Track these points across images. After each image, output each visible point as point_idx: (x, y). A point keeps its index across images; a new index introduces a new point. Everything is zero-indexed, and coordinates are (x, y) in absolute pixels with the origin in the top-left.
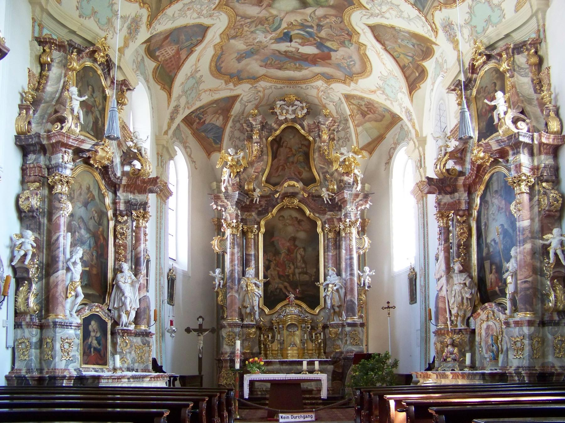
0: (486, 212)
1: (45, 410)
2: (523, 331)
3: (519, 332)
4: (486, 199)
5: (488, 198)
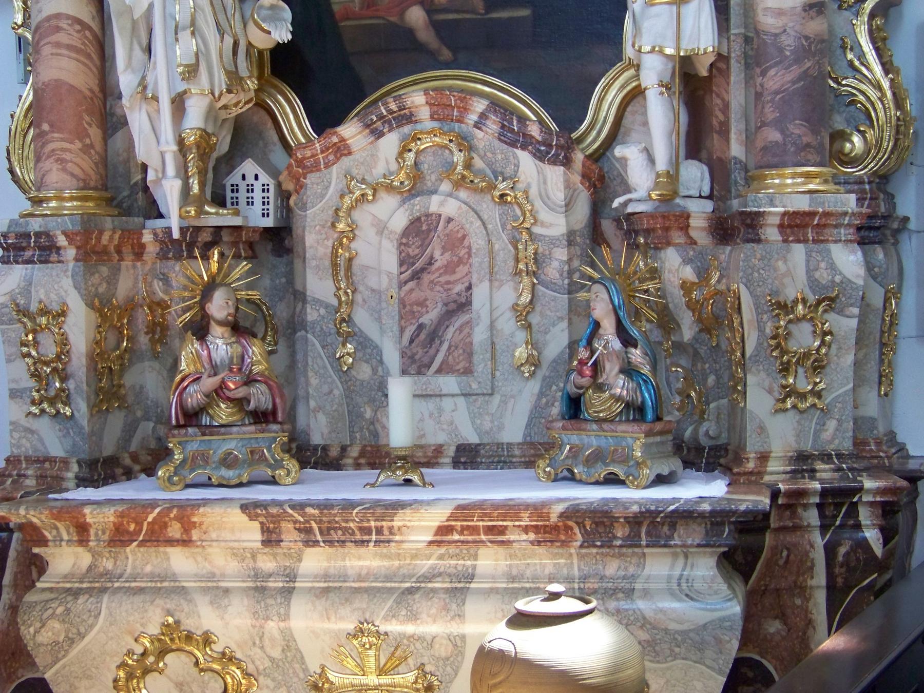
2: (832, 267)
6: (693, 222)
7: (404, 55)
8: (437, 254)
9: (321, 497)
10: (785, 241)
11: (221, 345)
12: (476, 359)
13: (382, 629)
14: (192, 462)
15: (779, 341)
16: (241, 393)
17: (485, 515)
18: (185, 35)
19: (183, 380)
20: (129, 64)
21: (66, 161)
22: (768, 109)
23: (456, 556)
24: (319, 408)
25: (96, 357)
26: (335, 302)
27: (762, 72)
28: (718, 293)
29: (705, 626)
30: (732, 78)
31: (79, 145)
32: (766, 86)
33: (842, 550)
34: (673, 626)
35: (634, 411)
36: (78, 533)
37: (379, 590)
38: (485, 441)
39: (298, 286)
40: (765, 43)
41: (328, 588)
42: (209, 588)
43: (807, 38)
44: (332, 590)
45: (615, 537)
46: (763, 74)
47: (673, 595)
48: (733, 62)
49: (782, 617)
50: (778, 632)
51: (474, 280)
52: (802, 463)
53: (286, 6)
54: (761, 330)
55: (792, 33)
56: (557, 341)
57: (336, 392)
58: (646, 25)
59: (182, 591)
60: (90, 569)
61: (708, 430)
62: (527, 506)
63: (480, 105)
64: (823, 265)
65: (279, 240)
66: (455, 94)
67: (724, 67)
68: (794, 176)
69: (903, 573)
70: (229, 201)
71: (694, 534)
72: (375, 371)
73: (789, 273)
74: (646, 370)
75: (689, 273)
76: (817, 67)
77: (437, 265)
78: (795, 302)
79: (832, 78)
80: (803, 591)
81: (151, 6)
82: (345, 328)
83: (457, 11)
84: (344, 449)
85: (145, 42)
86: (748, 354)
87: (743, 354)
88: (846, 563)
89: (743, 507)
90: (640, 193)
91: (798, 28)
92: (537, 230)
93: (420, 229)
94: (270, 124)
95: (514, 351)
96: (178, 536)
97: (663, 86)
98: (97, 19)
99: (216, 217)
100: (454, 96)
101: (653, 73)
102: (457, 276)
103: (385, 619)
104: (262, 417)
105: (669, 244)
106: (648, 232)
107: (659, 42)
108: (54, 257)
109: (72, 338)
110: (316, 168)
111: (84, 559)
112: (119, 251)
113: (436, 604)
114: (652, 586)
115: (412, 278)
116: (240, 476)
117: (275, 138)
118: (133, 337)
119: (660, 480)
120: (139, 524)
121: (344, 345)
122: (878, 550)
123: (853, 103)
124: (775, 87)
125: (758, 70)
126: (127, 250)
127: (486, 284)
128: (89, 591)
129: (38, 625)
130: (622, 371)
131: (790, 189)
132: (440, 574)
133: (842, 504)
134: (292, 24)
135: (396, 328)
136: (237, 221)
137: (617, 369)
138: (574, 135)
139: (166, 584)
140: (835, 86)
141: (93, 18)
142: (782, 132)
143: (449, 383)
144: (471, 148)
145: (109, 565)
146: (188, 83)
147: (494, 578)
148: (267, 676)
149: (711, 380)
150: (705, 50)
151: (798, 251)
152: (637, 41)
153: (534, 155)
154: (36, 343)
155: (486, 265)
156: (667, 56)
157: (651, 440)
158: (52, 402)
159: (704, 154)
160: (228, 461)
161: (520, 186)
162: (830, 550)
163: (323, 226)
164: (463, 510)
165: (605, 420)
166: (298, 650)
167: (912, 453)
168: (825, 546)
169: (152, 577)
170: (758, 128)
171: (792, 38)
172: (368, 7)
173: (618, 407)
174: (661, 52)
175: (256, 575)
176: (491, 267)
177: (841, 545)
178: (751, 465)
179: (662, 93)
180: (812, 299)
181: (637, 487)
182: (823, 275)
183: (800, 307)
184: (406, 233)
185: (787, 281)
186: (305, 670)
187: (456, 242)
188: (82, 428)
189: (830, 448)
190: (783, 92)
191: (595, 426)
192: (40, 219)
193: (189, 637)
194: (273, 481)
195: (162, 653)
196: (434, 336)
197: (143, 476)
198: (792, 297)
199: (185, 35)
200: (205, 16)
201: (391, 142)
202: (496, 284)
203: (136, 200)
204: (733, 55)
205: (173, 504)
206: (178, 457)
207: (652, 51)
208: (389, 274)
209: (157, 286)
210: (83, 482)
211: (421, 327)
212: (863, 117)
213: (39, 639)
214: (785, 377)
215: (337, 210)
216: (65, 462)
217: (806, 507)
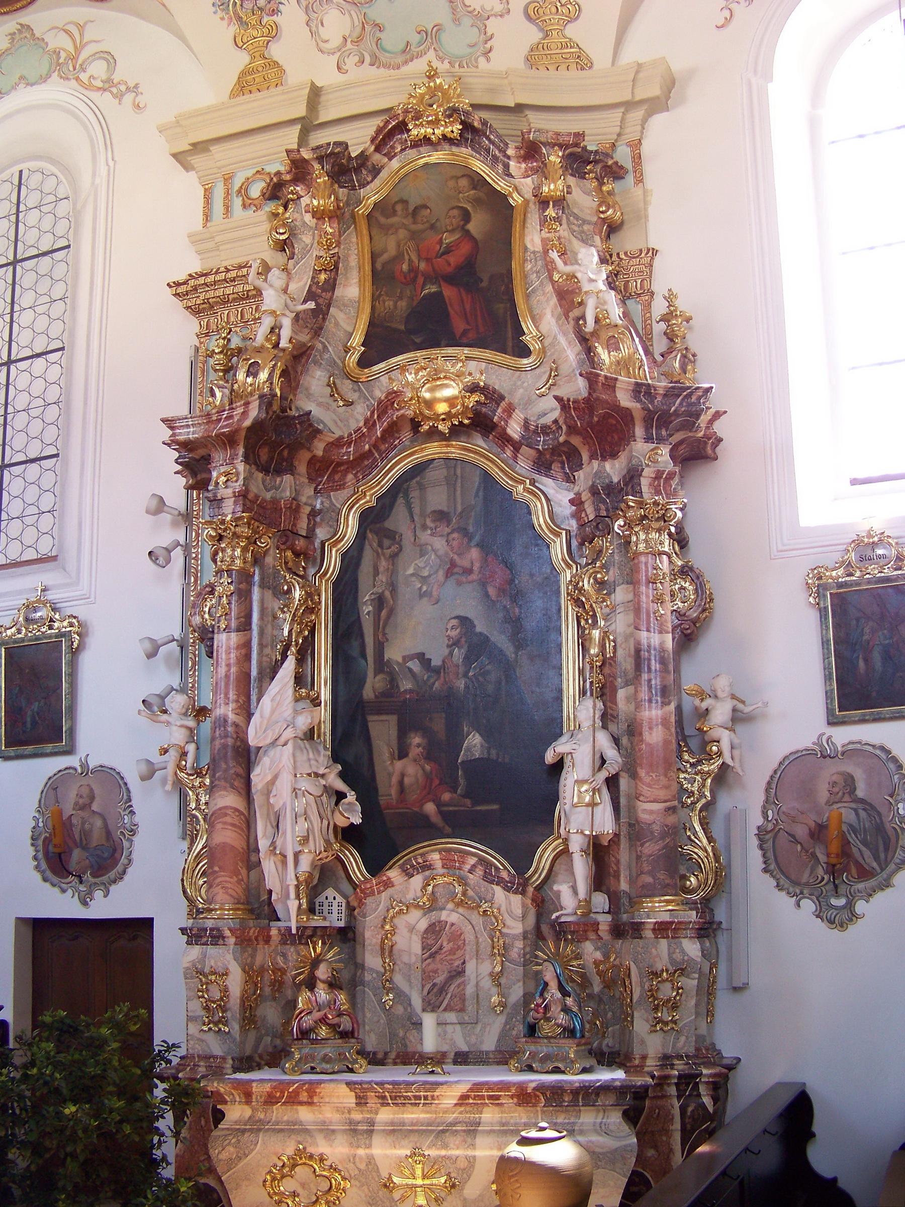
0: (383, 564)
1: (407, 852)
2: (683, 952)
3: (670, 955)
4: (389, 524)
5: (399, 520)
6: (601, 927)
7: (422, 830)
8: (445, 944)
9: (390, 1079)
10: (656, 938)
11: (322, 994)
12: (467, 1003)
13: (426, 1153)
14: (303, 1060)
15: (652, 993)
16: (336, 1021)
17: (490, 1088)
18: (301, 820)
19: (300, 1013)
20: (264, 835)
21: (227, 888)
22: (645, 865)
23: (470, 1112)
24: (371, 1030)
25: (243, 1000)
26: (382, 970)
28: (614, 966)
29: (616, 1150)
31: (235, 879)
33: (690, 1109)
34: (597, 1150)
35: (570, 1032)
36: (246, 1097)
37: (424, 1131)
38: (472, 1050)
39: (359, 961)
41: (393, 1130)
42: (323, 1129)
43: (667, 826)
44: (396, 1131)
45: (564, 1101)
46: (642, 845)
47: (596, 1131)
49: (655, 1147)
50: (653, 1155)
51: (467, 958)
52: (666, 1060)
54: (642, 987)
56: (517, 993)
57: (382, 1021)
58: (573, 818)
59: (307, 1131)
60: (250, 1117)
61: (608, 1043)
62: (514, 1084)
63: (472, 861)
64: (677, 951)
65: (347, 935)
68: (660, 902)
69: (721, 1125)
70: (317, 911)
71: (611, 1099)
72: (405, 1009)
73: (658, 956)
74: (575, 1009)
75: (598, 955)
77: (445, 950)
78: (662, 971)
80: (667, 1132)
82: (387, 984)
83: (455, 806)
84: (386, 1054)
85: (275, 824)
86: (634, 1001)
87: (631, 1000)
88: (692, 1116)
89: (639, 1083)
90: (569, 910)
91: (662, 820)
92: (505, 930)
93: (434, 930)
94: (340, 867)
95: (490, 999)
96: (305, 1100)
99: (317, 921)
101: (576, 844)
102: (455, 957)
103: (429, 1147)
104: (345, 1035)
105: (587, 939)
106: (572, 933)
107: (581, 827)
108: (221, 942)
109: (231, 988)
110: (372, 893)
111: (247, 1112)
112: (256, 939)
113: (458, 1140)
114: (585, 1128)
115: (430, 957)
116: (333, 1068)
117: (343, 875)
118: (269, 986)
119: (585, 1070)
120: (282, 1092)
121: (388, 995)
122: (711, 1110)
123: (691, 859)
124: (650, 852)
125: (639, 843)
126: (260, 938)
127: (474, 960)
128: (251, 1130)
129: (220, 1149)
130: (562, 1010)
131: (658, 909)
132: (460, 1122)
133: (689, 1084)
135: (420, 986)
136: (327, 924)
137: (559, 1009)
138: (527, 876)
139: (296, 1127)
142: (654, 878)
143: (451, 1017)
144: (466, 884)
145: (262, 1116)
147: (492, 1124)
148: (356, 1179)
149: (610, 1014)
151: (664, 943)
153: (504, 889)
154: (207, 990)
155: (474, 950)
157: (580, 1048)
158: (216, 1024)
159: (604, 888)
160: (326, 1059)
161: (495, 905)
162: (683, 1109)
163: (376, 927)
164: (477, 1086)
165: (551, 1037)
166: (376, 1164)
167: (724, 1055)
168: (680, 1107)
169: (288, 1123)
170: (638, 876)
173: (559, 1030)
174: (582, 832)
175: (350, 1123)
176: (477, 951)
177: (688, 1106)
178: (637, 1062)
180: (671, 970)
181: (572, 1074)
182: (678, 956)
183: (665, 974)
184: (426, 931)
185: (657, 959)
186: (379, 1176)
187: (456, 936)
188: (235, 1039)
189: (682, 1052)
191: (545, 1041)
192: (212, 921)
193: (311, 1157)
194: (351, 1071)
195: (294, 1166)
196: (442, 990)
197: (266, 1067)
198: (660, 969)
199: (301, 820)
201: (417, 881)
202: (480, 961)
203: (264, 910)
205: (305, 1082)
206: (297, 1056)
207: (577, 832)
208: (416, 955)
209: (280, 960)
210: (236, 1070)
211: (434, 985)
212: (696, 867)
213: (221, 1157)
214: (656, 1013)
215: (385, 918)
216: (224, 1059)
217: (669, 1085)
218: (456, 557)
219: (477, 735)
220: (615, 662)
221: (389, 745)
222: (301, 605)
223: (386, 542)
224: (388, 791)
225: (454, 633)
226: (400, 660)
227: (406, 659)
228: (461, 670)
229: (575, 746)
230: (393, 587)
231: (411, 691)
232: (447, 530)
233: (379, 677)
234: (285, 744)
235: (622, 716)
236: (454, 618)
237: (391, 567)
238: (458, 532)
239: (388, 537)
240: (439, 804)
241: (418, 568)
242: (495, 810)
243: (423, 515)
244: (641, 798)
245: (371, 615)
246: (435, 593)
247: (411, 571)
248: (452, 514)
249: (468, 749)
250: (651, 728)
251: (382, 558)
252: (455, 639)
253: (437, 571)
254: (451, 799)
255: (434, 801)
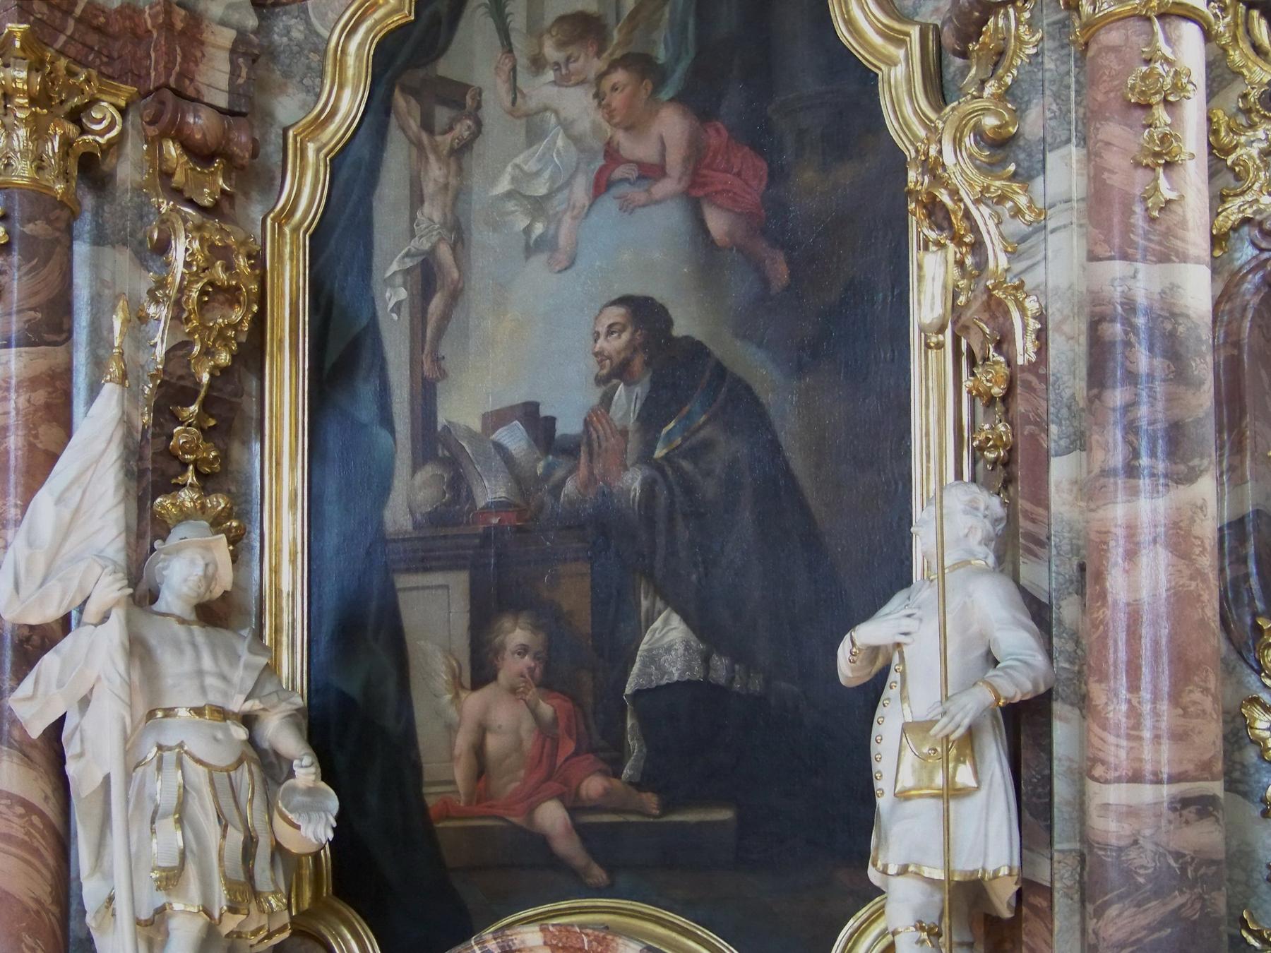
4: (447, 67)
27: (1095, 910)
30: (1057, 924)
32: (1102, 934)
40: (1102, 863)
43: (1178, 855)
46: (1099, 913)
48: (1057, 896)
53: (332, 792)
55: (1149, 847)
66: (589, 931)
67: (1045, 904)
76: (1198, 906)
79: (1250, 931)
81: (107, 779)
83: (615, 811)
97: (922, 929)
98: (53, 800)
100: (587, 935)
124: (1120, 936)
134: (338, 819)
140: (1257, 944)
141: (46, 798)
146: (169, 895)
150: (996, 872)
152: (880, 856)
156: (931, 882)
171: (1150, 855)
172: (478, 802)
179: (921, 942)
190: (1133, 944)
199: (167, 826)
200: (201, 798)
204: (1057, 885)
207: (903, 871)
218: (621, 137)
219: (676, 620)
220: (1044, 379)
221: (449, 652)
222: (196, 276)
223: (442, 115)
224: (445, 768)
225: (615, 344)
226: (476, 425)
227: (496, 419)
228: (634, 445)
229: (907, 625)
230: (458, 233)
231: (499, 506)
232: (598, 65)
233: (421, 476)
234: (105, 618)
235: (1060, 537)
236: (614, 303)
237: (453, 181)
238: (626, 67)
239: (445, 102)
240: (575, 807)
241: (524, 177)
242: (723, 823)
243: (534, 31)
244: (1098, 771)
245: (405, 310)
246: (563, 240)
247: (504, 185)
248: (611, 20)
249: (652, 659)
250: (1131, 554)
251: (432, 158)
252: (616, 361)
253: (568, 184)
254: (607, 793)
255: (561, 797)
